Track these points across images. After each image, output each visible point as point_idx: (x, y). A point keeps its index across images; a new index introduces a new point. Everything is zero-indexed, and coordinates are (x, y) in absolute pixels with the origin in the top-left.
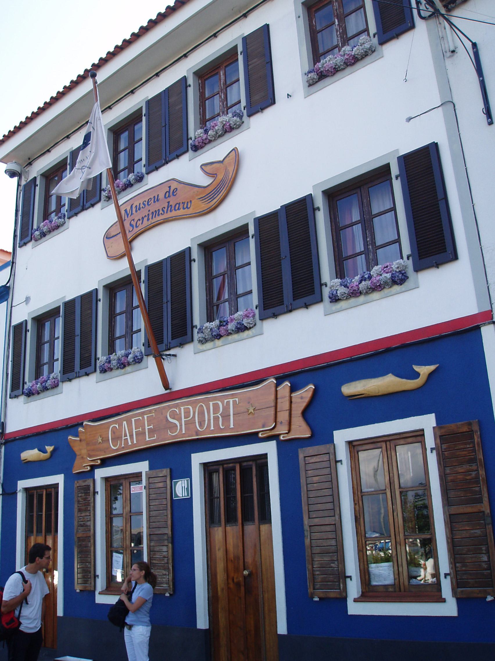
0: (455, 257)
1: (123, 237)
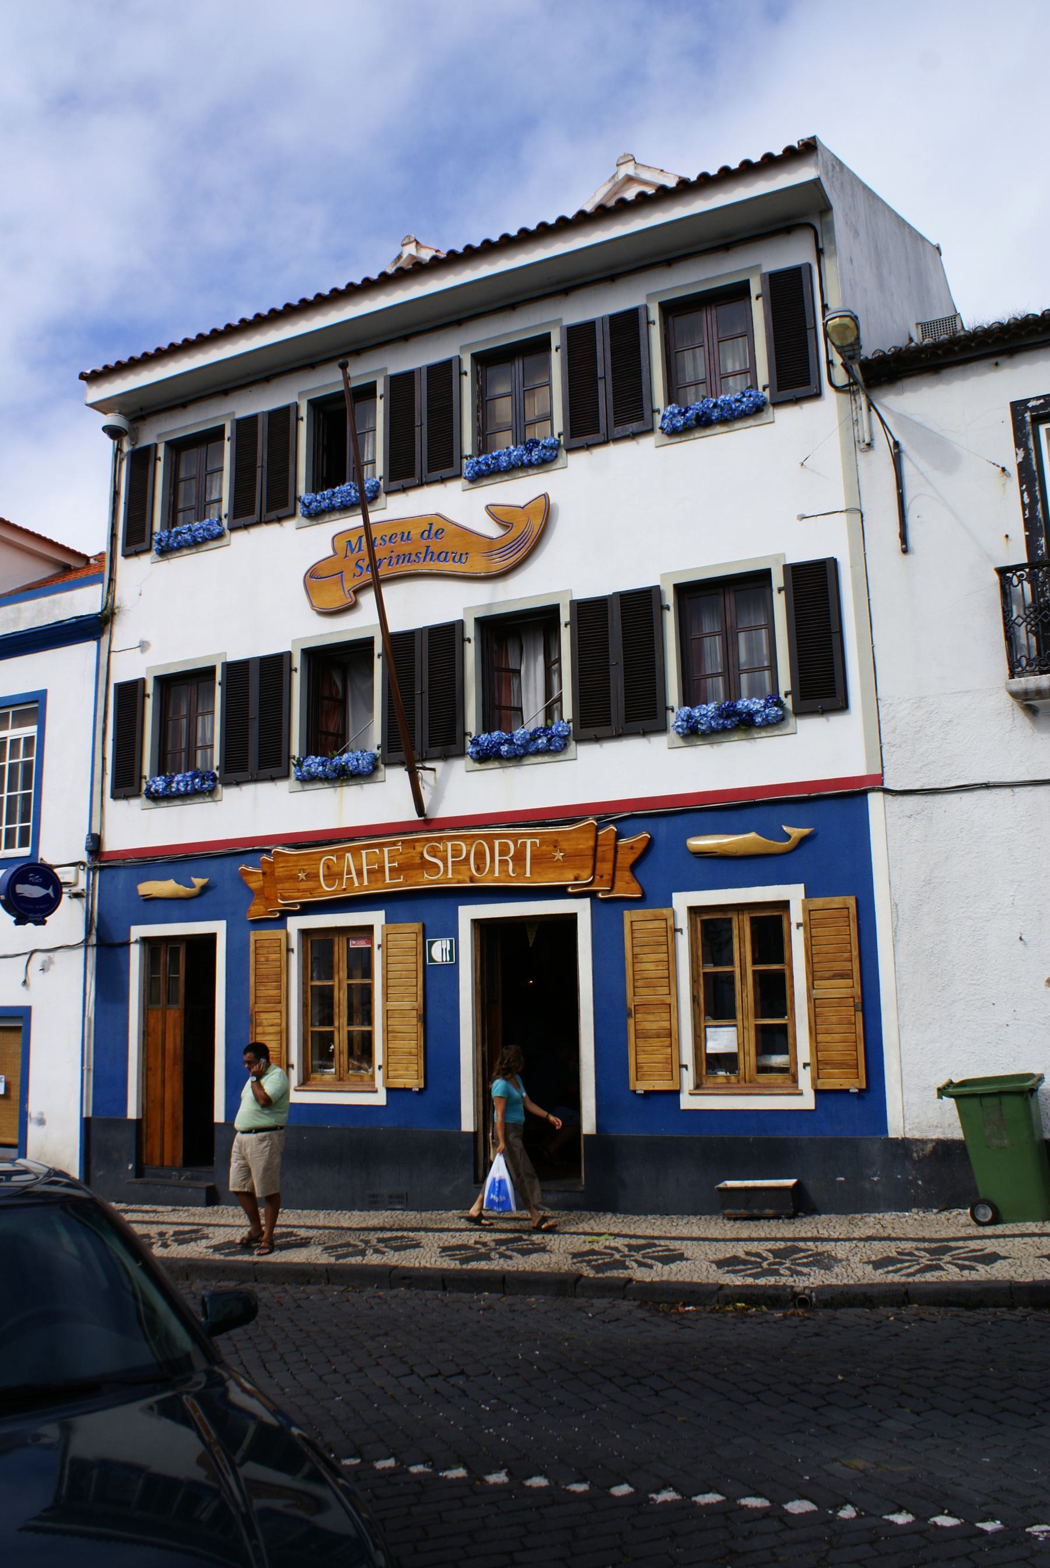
0: (843, 706)
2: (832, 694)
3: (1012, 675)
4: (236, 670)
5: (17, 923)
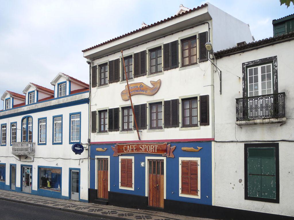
1: (129, 93)
2: (206, 122)
3: (237, 121)
4: (111, 110)
5: (76, 154)
